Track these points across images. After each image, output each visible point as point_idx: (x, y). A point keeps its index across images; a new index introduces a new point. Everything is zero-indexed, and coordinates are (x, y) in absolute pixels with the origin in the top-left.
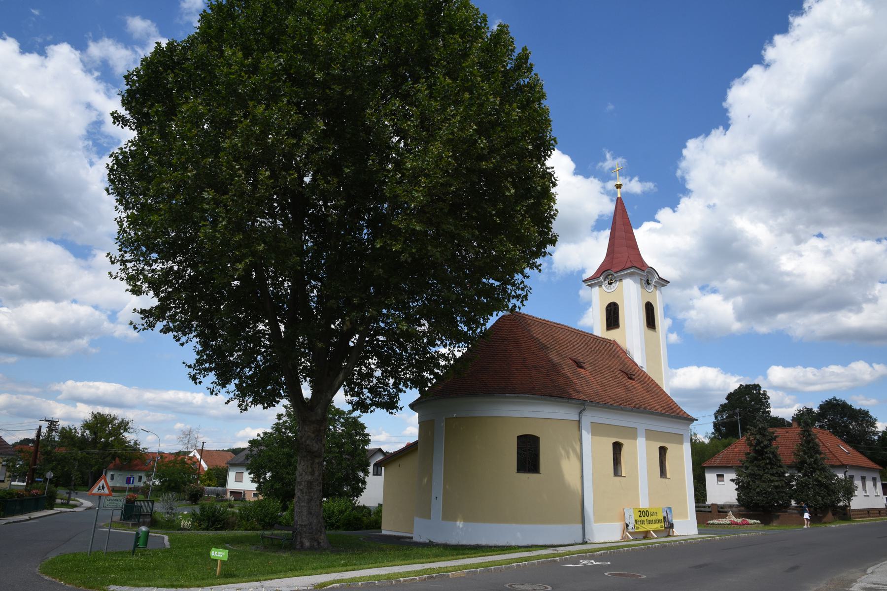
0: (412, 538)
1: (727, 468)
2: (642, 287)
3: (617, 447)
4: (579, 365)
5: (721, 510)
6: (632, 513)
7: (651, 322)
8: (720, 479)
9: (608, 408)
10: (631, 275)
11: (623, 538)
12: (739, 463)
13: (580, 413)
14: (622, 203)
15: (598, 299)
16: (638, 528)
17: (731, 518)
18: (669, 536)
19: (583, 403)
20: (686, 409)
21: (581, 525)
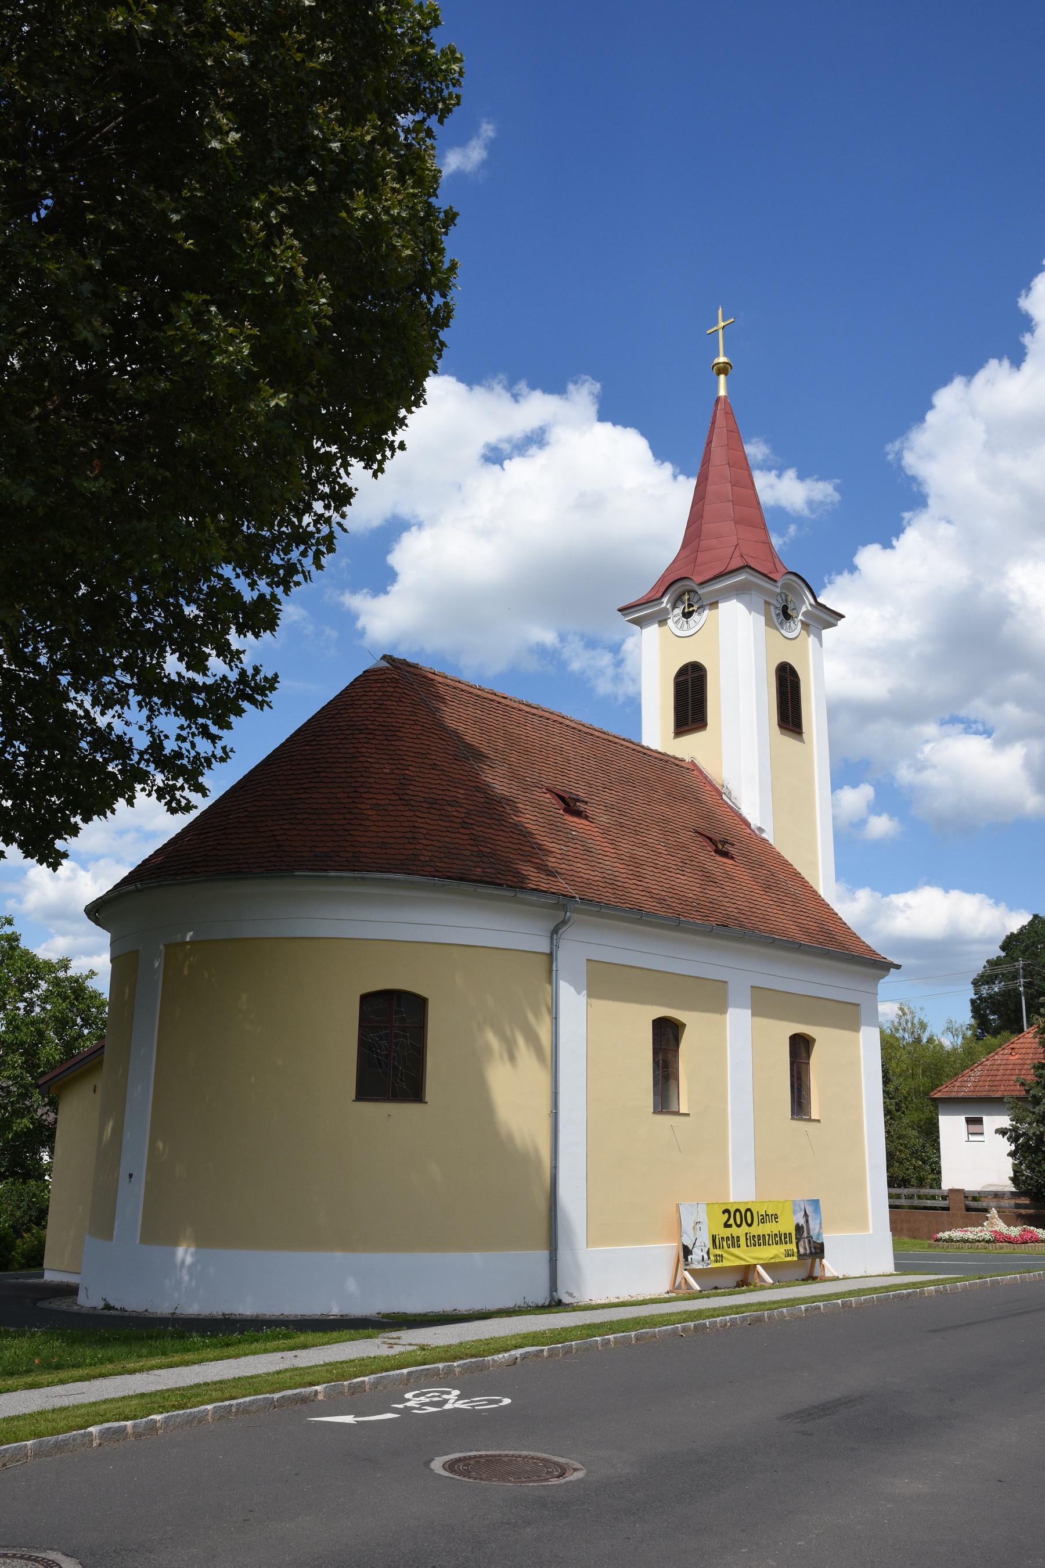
0: (71, 1291)
1: (993, 1103)
2: (769, 623)
3: (667, 1035)
4: (571, 806)
5: (973, 1206)
6: (703, 1217)
7: (789, 714)
8: (974, 1128)
9: (640, 921)
10: (739, 591)
11: (675, 1288)
12: (1019, 1091)
13: (555, 931)
14: (729, 413)
15: (654, 656)
16: (719, 1258)
17: (996, 1225)
18: (811, 1278)
19: (564, 906)
20: (890, 959)
21: (544, 1255)
